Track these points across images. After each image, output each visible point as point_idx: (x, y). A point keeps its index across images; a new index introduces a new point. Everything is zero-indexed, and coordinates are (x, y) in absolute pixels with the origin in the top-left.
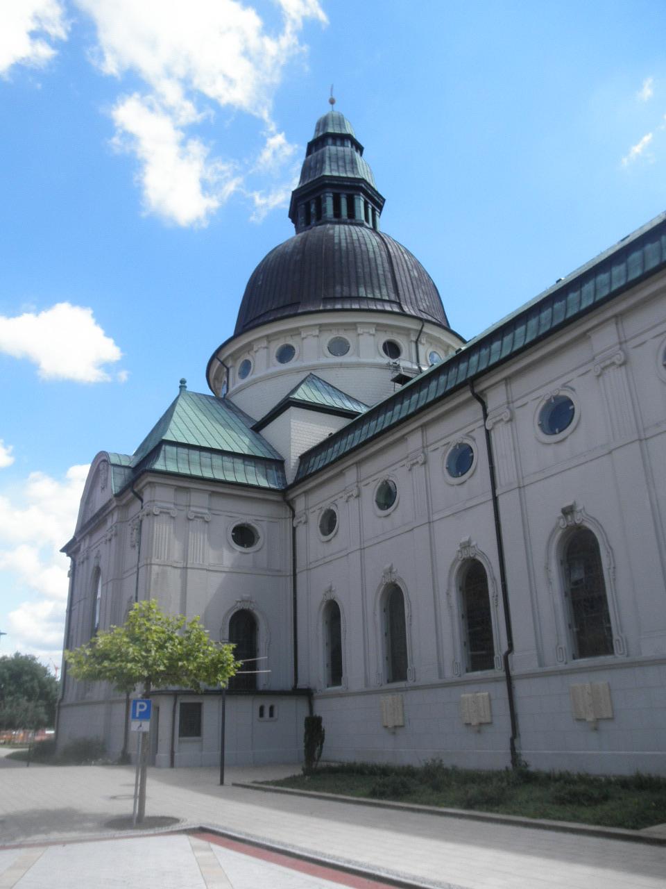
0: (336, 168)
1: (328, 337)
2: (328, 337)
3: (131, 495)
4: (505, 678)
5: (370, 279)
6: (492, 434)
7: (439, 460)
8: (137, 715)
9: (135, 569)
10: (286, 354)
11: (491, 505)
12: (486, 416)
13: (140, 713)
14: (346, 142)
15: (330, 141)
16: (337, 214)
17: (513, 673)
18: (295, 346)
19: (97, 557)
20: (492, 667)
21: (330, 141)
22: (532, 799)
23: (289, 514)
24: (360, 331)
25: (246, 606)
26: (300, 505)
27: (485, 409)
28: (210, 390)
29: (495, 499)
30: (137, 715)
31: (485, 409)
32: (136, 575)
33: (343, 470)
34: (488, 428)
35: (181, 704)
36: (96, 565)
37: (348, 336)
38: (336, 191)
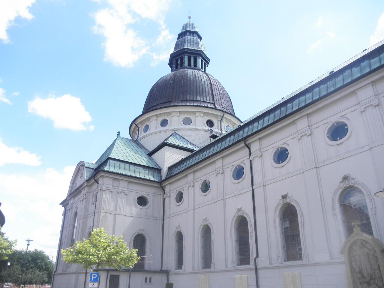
1: (183, 117)
2: (183, 117)
4: (254, 269)
5: (202, 93)
6: (253, 162)
7: (198, 185)
8: (92, 280)
10: (164, 123)
12: (250, 154)
13: (94, 278)
14: (195, 35)
15: (188, 34)
16: (189, 64)
17: (258, 267)
20: (249, 264)
21: (188, 34)
23: (162, 193)
24: (197, 115)
25: (141, 232)
26: (167, 189)
27: (250, 151)
30: (92, 280)
31: (250, 151)
34: (251, 159)
35: (111, 275)
37: (191, 117)
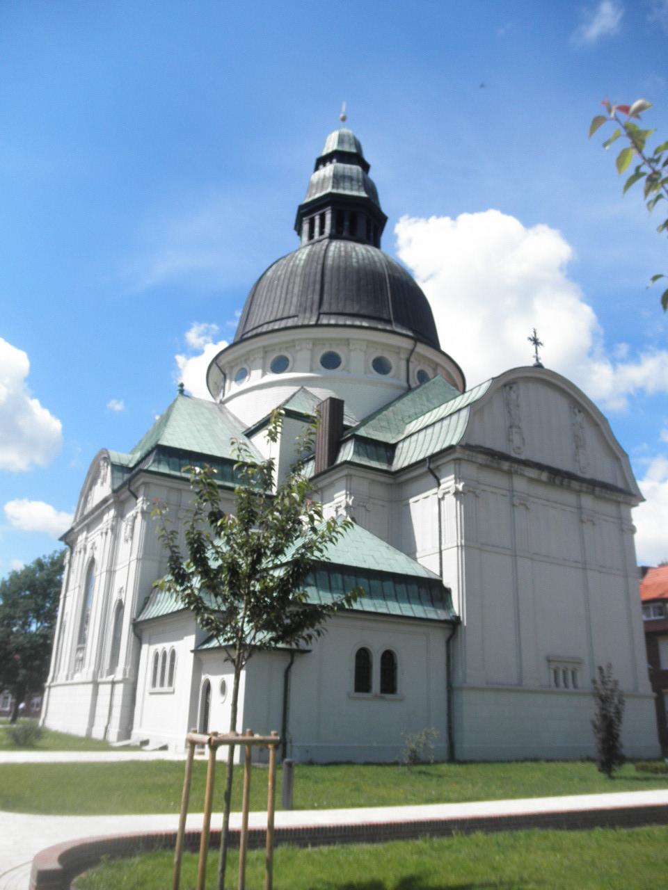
0: (349, 187)
3: (128, 493)
9: (128, 563)
11: (438, 555)
18: (290, 359)
19: (92, 548)
22: (477, 846)
28: (210, 395)
29: (441, 552)
32: (127, 567)
33: (333, 481)
36: (91, 556)
38: (309, 217)
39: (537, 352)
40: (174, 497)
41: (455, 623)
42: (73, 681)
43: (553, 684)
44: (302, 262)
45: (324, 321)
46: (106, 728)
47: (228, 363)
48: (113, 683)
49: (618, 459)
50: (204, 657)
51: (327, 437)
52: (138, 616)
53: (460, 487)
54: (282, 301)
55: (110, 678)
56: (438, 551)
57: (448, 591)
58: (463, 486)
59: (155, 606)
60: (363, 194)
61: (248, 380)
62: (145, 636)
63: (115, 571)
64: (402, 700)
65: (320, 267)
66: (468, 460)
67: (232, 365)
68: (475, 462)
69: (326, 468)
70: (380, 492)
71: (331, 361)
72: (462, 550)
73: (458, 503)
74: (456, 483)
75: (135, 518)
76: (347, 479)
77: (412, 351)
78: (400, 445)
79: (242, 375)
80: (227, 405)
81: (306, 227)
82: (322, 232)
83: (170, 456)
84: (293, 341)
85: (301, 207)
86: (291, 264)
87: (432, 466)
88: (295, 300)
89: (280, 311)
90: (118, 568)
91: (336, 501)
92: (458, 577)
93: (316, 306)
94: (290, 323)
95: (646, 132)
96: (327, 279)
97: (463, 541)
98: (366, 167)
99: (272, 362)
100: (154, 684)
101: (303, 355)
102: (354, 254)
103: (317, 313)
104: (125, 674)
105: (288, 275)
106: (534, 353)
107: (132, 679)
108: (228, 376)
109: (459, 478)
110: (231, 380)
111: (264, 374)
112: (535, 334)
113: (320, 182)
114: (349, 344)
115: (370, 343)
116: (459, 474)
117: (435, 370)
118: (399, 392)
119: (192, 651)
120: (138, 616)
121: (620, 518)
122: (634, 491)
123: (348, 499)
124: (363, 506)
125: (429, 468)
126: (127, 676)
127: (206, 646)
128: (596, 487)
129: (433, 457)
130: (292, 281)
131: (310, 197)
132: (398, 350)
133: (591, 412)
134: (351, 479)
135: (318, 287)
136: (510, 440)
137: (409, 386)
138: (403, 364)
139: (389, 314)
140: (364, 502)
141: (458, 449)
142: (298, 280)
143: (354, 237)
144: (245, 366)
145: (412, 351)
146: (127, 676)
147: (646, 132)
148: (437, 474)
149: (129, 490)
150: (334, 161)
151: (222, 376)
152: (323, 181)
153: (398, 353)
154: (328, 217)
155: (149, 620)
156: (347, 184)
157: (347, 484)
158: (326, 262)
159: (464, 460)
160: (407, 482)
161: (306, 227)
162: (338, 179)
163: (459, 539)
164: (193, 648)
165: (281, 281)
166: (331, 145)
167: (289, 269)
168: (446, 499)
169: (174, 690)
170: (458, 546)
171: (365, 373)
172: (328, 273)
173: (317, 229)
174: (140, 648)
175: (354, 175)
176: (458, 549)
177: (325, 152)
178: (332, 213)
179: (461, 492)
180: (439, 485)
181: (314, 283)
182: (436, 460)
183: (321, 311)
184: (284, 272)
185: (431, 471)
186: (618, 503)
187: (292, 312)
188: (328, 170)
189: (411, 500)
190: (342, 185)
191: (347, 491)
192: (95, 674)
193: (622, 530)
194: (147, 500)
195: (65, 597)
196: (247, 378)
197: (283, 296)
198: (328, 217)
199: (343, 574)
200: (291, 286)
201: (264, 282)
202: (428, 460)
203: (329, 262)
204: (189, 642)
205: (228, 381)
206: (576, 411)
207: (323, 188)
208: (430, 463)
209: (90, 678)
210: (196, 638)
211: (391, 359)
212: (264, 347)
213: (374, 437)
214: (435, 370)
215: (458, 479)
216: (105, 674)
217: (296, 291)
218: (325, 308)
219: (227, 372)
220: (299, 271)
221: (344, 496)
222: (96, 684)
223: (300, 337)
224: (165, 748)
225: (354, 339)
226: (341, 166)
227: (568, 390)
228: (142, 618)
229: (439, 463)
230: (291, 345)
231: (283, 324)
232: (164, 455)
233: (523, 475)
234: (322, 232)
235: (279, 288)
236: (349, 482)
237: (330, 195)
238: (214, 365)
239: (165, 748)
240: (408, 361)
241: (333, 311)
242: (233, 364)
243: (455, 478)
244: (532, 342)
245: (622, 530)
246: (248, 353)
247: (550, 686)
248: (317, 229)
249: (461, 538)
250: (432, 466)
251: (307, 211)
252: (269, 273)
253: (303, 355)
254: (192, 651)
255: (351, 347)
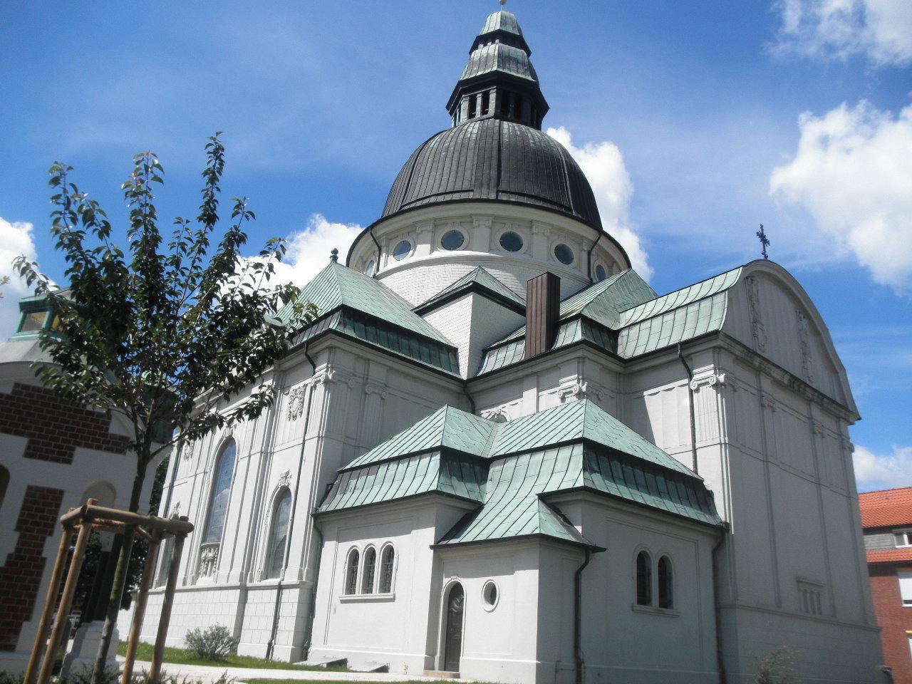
3: (303, 357)
11: (691, 454)
29: (695, 450)
39: (764, 250)
40: (361, 368)
41: (721, 531)
42: (193, 587)
43: (803, 608)
44: (474, 136)
45: (504, 197)
46: (270, 644)
47: (387, 234)
48: (280, 588)
49: (835, 372)
50: (447, 555)
51: (544, 316)
52: (320, 503)
53: (722, 378)
54: (453, 174)
55: (274, 581)
56: (691, 448)
57: (710, 495)
58: (725, 377)
59: (348, 494)
60: (530, 78)
61: (412, 256)
62: (326, 533)
63: (272, 453)
64: (676, 617)
65: (495, 142)
66: (726, 350)
67: (390, 237)
68: (733, 354)
69: (543, 350)
70: (609, 381)
71: (511, 243)
72: (726, 449)
73: (719, 395)
74: (715, 373)
75: (314, 388)
76: (579, 363)
77: (595, 243)
78: (624, 333)
79: (403, 249)
80: (383, 281)
81: (465, 105)
82: (484, 111)
83: (355, 321)
84: (471, 215)
85: (461, 83)
86: (461, 136)
87: (683, 354)
88: (468, 174)
89: (422, 191)
90: (276, 450)
91: (563, 386)
92: (723, 479)
93: (493, 183)
94: (464, 196)
95: (200, 219)
96: (504, 156)
97: (726, 438)
98: (529, 53)
99: (446, 233)
100: (350, 588)
101: (482, 233)
102: (529, 135)
103: (496, 190)
104: (300, 576)
105: (458, 147)
106: (762, 250)
107: (310, 584)
108: (384, 249)
109: (719, 369)
110: (388, 254)
111: (432, 250)
112: (762, 230)
113: (483, 60)
114: (531, 228)
115: (556, 230)
116: (719, 364)
117: (610, 267)
118: (585, 285)
119: (432, 547)
120: (320, 503)
121: (840, 435)
122: (850, 407)
123: (580, 384)
124: (595, 394)
125: (680, 355)
126: (304, 580)
127: (445, 542)
128: (821, 399)
129: (685, 345)
130: (463, 153)
131: (485, 70)
132: (580, 240)
133: (815, 320)
134: (583, 363)
135: (495, 163)
136: (755, 336)
137: (591, 279)
138: (585, 256)
139: (570, 203)
140: (597, 390)
141: (721, 336)
142: (470, 153)
143: (518, 119)
144: (409, 240)
145: (595, 243)
146: (304, 580)
147: (200, 219)
148: (689, 364)
149: (306, 354)
150: (497, 41)
151: (377, 248)
152: (486, 60)
153: (580, 244)
154: (493, 97)
155: (335, 511)
156: (513, 66)
157: (578, 366)
158: (501, 139)
159: (724, 348)
160: (640, 371)
161: (465, 105)
162: (503, 58)
163: (722, 435)
164: (432, 543)
165: (450, 154)
166: (493, 23)
167: (460, 141)
168: (701, 391)
169: (394, 595)
170: (721, 444)
171: (548, 260)
172: (504, 150)
173: (478, 108)
174: (322, 545)
175: (520, 58)
176: (721, 447)
177: (485, 31)
178: (497, 92)
179: (722, 384)
180: (691, 377)
181: (491, 158)
182: (687, 348)
183: (500, 189)
184: (453, 143)
185: (683, 360)
186: (839, 418)
187: (466, 186)
188: (492, 49)
189: (646, 393)
190: (507, 65)
191: (579, 375)
192: (243, 578)
193: (843, 448)
194: (332, 368)
195: (172, 486)
196: (411, 252)
197: (454, 168)
198: (493, 97)
199: (621, 461)
200: (462, 159)
201: (427, 153)
202: (679, 346)
203: (505, 139)
204: (427, 536)
205: (384, 254)
206: (802, 316)
207: (486, 66)
208: (681, 349)
209: (235, 581)
210: (436, 531)
211: (574, 249)
212: (435, 219)
213: (599, 321)
214: (610, 267)
215: (718, 369)
216: (257, 575)
217: (469, 164)
218: (503, 186)
219: (383, 244)
220: (472, 144)
221: (576, 381)
222: (244, 590)
223: (477, 212)
224: (384, 669)
225: (538, 222)
226: (506, 47)
227: (796, 292)
228: (324, 508)
229: (692, 350)
230: (469, 220)
231: (448, 198)
232: (349, 318)
233: (769, 374)
234: (484, 111)
235: (448, 160)
236: (581, 364)
237: (496, 72)
238: (368, 234)
239: (384, 669)
240: (589, 254)
241: (512, 190)
242: (390, 237)
243: (715, 369)
244: (760, 239)
245: (843, 448)
246: (414, 224)
247: (801, 610)
248: (478, 108)
249: (725, 436)
250: (684, 354)
251: (467, 88)
252: (432, 144)
253: (482, 233)
254: (432, 547)
255: (534, 230)
